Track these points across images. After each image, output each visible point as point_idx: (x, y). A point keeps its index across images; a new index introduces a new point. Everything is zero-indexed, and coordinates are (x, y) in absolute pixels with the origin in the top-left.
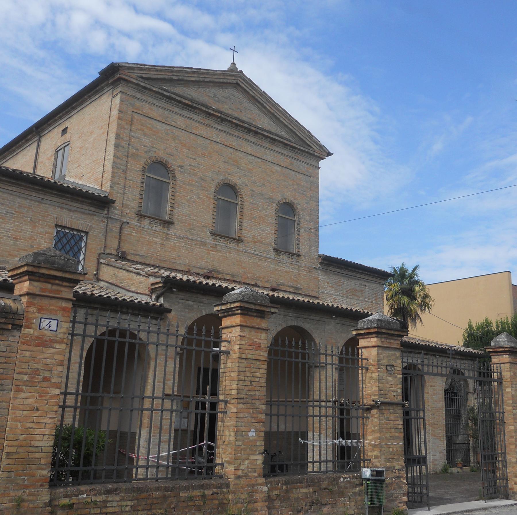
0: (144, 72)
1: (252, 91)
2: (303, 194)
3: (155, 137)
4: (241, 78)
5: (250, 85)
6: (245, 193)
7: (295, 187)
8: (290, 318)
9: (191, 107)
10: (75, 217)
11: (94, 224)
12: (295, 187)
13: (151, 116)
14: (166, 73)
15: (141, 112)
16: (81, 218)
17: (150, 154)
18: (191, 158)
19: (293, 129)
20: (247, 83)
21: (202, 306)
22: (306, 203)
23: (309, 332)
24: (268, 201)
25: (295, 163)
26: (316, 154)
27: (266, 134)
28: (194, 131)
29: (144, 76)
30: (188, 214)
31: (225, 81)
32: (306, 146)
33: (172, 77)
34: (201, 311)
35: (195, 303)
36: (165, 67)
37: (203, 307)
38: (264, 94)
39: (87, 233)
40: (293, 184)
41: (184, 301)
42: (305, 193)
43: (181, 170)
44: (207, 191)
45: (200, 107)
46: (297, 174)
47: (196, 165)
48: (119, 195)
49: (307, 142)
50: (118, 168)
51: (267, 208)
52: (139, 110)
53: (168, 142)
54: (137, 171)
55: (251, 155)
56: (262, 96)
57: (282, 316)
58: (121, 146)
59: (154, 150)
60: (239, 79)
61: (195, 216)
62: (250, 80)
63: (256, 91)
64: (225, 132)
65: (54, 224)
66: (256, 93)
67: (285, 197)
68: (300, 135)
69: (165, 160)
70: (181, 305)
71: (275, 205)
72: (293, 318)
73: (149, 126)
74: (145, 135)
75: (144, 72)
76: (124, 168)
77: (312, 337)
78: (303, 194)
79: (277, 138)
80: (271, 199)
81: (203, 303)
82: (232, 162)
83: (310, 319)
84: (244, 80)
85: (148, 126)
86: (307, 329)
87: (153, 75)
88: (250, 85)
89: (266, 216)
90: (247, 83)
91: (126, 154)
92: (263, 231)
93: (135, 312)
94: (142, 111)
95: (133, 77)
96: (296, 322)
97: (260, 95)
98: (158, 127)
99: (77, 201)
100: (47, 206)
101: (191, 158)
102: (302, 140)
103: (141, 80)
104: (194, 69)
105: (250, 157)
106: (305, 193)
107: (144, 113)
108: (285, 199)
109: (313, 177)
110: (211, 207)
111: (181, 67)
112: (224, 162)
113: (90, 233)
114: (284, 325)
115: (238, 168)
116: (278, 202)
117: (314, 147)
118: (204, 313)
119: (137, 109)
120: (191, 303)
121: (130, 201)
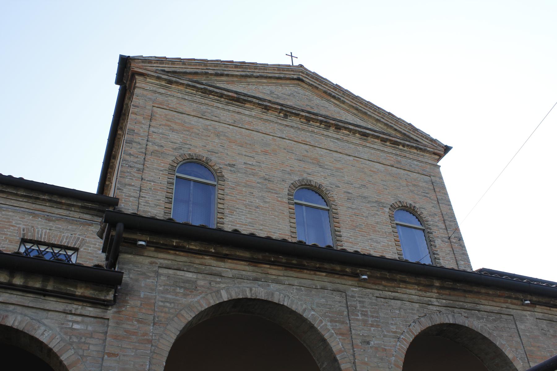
0: (167, 66)
1: (322, 86)
2: (425, 196)
3: (188, 133)
4: (302, 72)
5: (317, 79)
6: (337, 196)
7: (411, 188)
8: (435, 308)
9: (239, 100)
10: (56, 227)
11: (88, 237)
12: (411, 188)
13: (181, 110)
14: (198, 67)
15: (165, 107)
16: (68, 230)
17: (181, 151)
18: (245, 155)
19: (388, 123)
20: (312, 77)
21: (219, 283)
22: (433, 207)
23: (487, 336)
24: (376, 205)
25: (403, 160)
26: (428, 149)
27: (351, 127)
28: (247, 127)
29: (166, 69)
30: (250, 223)
31: (282, 76)
32: (412, 141)
33: (206, 71)
34: (218, 292)
35: (200, 276)
36: (194, 59)
37: (223, 286)
38: (337, 88)
39: (76, 250)
40: (407, 185)
41: (171, 272)
42: (428, 195)
43: (232, 169)
44: (276, 193)
45: (250, 99)
46: (409, 173)
47: (254, 163)
48: (131, 199)
49: (412, 136)
50: (131, 167)
51: (377, 214)
52: (163, 105)
53: (209, 138)
54: (161, 170)
55: (336, 152)
56: (336, 90)
57: (417, 305)
58: (136, 142)
59: (187, 146)
60: (301, 74)
61: (262, 225)
62: (314, 73)
63: (327, 86)
64: (292, 127)
65: (18, 239)
66: (327, 87)
67: (400, 200)
68: (400, 130)
69: (205, 158)
70: (162, 278)
71: (387, 210)
72: (443, 309)
73: (179, 121)
74: (173, 130)
75: (167, 66)
76: (141, 166)
77: (495, 345)
78: (425, 196)
79: (368, 131)
80: (380, 204)
81: (221, 276)
82: (310, 161)
83: (479, 311)
84: (307, 74)
85: (177, 121)
86: (479, 331)
87: (178, 68)
88: (317, 79)
89: (377, 223)
90: (312, 77)
91: (144, 150)
92: (377, 242)
93: (31, 284)
94: (168, 106)
95: (149, 69)
96: (450, 316)
97: (333, 89)
98: (193, 123)
99: (60, 204)
100: (10, 213)
101: (245, 155)
102: (405, 134)
103: (162, 72)
104: (236, 62)
105: (335, 154)
106: (428, 195)
107: (170, 107)
108: (400, 202)
109: (433, 176)
110: (286, 213)
111: (217, 61)
112: (297, 160)
113: (81, 250)
114: (427, 323)
115: (321, 166)
116: (391, 206)
117: (424, 142)
118: (225, 297)
119: (161, 104)
120: (189, 275)
121: (150, 206)
